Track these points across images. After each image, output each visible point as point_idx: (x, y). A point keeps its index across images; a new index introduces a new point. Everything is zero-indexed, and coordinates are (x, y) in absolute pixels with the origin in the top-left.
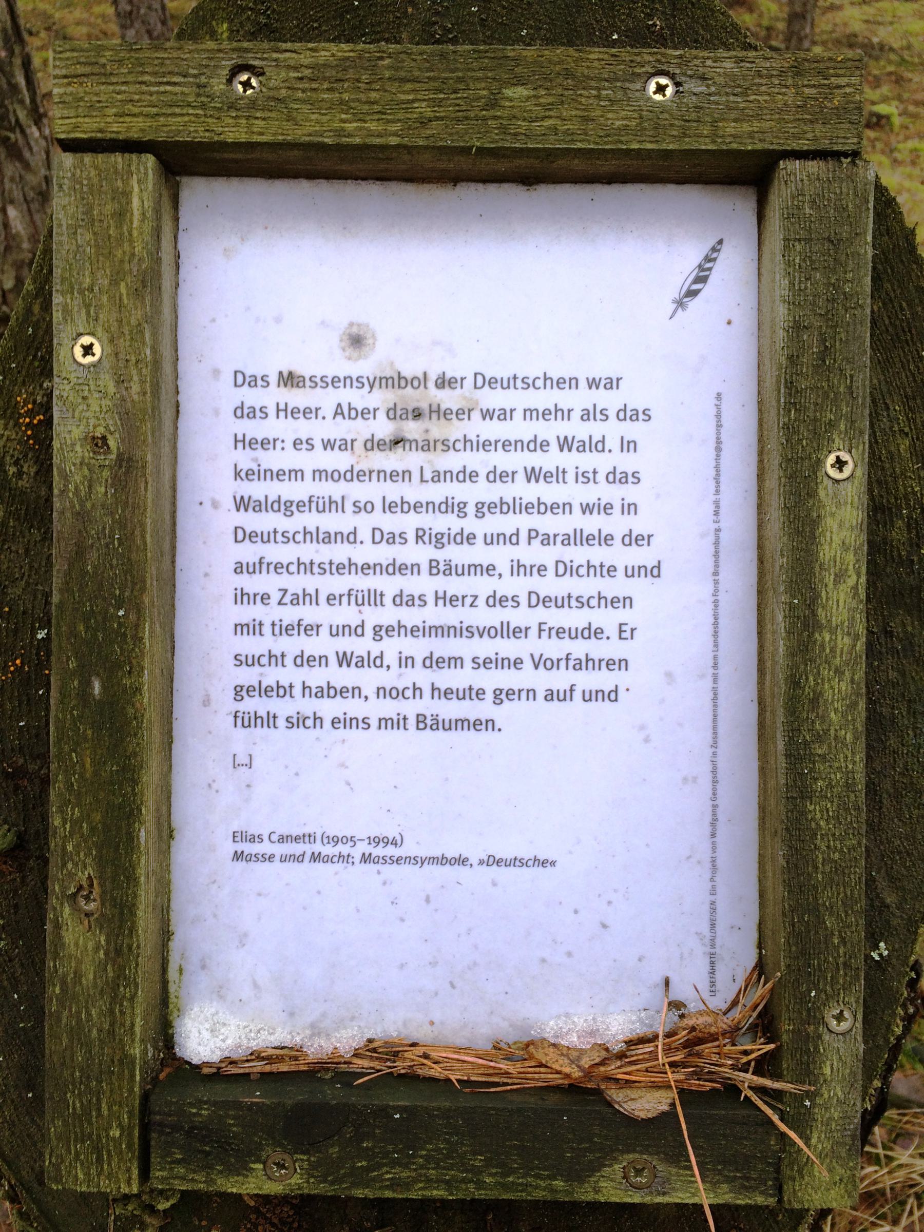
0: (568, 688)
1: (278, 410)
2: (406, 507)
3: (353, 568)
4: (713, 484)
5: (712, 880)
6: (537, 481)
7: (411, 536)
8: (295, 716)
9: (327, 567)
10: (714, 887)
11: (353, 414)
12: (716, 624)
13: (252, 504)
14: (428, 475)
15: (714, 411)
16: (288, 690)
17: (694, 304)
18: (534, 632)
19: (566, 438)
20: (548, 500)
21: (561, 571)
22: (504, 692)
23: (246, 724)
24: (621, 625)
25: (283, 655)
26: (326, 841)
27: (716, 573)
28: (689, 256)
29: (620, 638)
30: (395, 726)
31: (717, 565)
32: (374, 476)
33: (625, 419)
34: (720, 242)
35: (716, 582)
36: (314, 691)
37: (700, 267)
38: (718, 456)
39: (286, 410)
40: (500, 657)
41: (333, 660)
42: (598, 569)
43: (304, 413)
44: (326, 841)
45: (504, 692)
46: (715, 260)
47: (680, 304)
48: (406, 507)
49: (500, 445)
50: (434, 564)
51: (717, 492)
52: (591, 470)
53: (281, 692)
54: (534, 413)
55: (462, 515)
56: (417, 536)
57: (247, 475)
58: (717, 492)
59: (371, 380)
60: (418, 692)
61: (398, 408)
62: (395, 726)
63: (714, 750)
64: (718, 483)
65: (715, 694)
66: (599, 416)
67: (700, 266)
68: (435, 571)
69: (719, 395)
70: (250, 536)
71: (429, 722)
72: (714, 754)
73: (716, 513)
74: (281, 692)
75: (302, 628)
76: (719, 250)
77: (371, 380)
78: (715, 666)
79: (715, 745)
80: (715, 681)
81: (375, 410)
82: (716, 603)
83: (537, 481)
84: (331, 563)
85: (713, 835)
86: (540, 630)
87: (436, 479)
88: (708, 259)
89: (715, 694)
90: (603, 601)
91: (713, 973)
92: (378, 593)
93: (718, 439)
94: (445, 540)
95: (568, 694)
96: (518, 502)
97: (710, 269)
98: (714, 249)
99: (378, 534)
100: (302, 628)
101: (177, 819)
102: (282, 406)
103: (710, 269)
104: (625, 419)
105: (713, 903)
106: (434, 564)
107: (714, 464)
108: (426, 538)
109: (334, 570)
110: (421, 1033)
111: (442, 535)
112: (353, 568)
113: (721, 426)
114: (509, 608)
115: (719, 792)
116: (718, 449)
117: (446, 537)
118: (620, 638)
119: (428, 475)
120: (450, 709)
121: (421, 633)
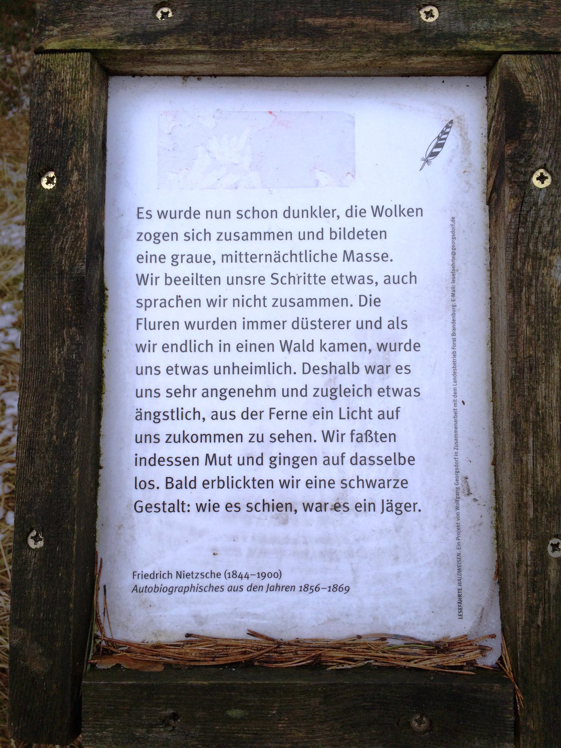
0: (395, 410)
3: (290, 437)
4: (451, 325)
5: (458, 539)
6: (381, 216)
8: (191, 232)
10: (459, 544)
11: (402, 461)
12: (455, 367)
13: (293, 346)
17: (435, 161)
18: (266, 415)
20: (189, 432)
25: (264, 299)
26: (227, 576)
27: (454, 334)
29: (139, 218)
30: (271, 508)
31: (454, 329)
32: (263, 258)
34: (451, 122)
35: (454, 340)
36: (338, 369)
38: (453, 258)
40: (367, 502)
41: (278, 347)
43: (184, 281)
44: (227, 576)
45: (300, 459)
46: (448, 133)
47: (427, 161)
50: (169, 480)
51: (454, 281)
52: (317, 320)
54: (268, 324)
57: (408, 212)
58: (454, 281)
61: (358, 457)
62: (271, 508)
63: (456, 451)
65: (456, 414)
66: (400, 326)
67: (438, 137)
71: (175, 483)
72: (456, 454)
73: (453, 295)
76: (450, 127)
79: (456, 447)
82: (454, 354)
83: (381, 216)
84: (320, 321)
86: (271, 413)
88: (443, 133)
90: (325, 257)
91: (460, 603)
92: (180, 502)
93: (453, 246)
94: (337, 393)
95: (395, 413)
97: (445, 139)
98: (447, 127)
99: (306, 366)
101: (432, 77)
103: (445, 139)
109: (204, 282)
110: (106, 385)
111: (336, 389)
114: (153, 513)
116: (454, 254)
117: (338, 391)
118: (139, 218)
119: (344, 415)
121: (244, 349)
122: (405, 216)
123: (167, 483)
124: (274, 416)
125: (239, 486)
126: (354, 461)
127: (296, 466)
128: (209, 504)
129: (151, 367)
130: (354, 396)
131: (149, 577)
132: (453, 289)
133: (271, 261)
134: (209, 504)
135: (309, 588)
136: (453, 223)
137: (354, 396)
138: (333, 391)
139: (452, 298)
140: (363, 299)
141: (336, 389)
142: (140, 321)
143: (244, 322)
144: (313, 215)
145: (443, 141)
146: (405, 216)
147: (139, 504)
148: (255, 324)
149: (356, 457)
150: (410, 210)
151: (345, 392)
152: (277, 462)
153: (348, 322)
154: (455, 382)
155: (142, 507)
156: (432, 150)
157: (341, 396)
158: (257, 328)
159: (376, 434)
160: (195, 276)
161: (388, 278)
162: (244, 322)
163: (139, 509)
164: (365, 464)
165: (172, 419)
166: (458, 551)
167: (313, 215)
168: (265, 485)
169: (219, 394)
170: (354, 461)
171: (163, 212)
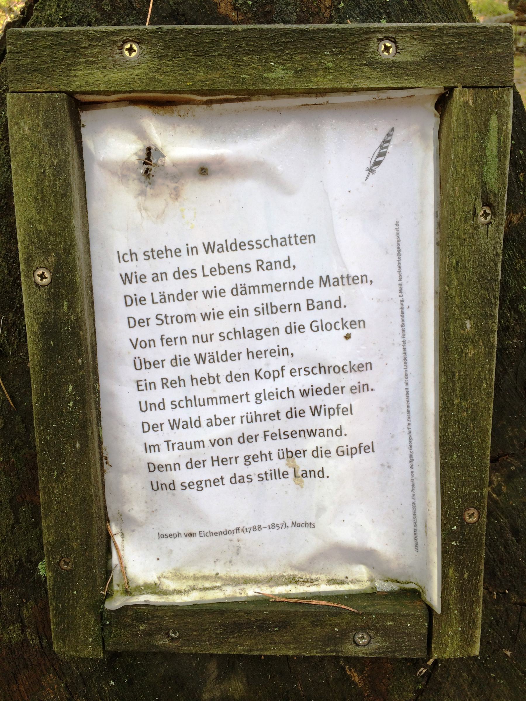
1: (213, 461)
2: (222, 271)
3: (169, 252)
5: (412, 491)
7: (253, 266)
9: (150, 254)
11: (274, 310)
13: (216, 247)
14: (157, 299)
15: (395, 232)
16: (216, 378)
17: (378, 170)
19: (209, 243)
21: (129, 302)
22: (263, 331)
23: (250, 420)
24: (265, 432)
27: (403, 325)
28: (374, 141)
29: (139, 390)
31: (403, 321)
33: (236, 483)
34: (392, 130)
37: (381, 147)
38: (399, 258)
39: (218, 461)
42: (268, 456)
45: (263, 331)
46: (389, 141)
47: (371, 171)
48: (222, 271)
49: (268, 353)
50: (310, 302)
51: (400, 279)
52: (263, 473)
53: (212, 380)
54: (269, 287)
55: (200, 489)
56: (258, 266)
57: (351, 325)
58: (400, 279)
59: (213, 442)
60: (134, 256)
61: (237, 477)
63: (409, 422)
64: (400, 273)
68: (311, 307)
69: (397, 222)
70: (153, 428)
72: (411, 453)
73: (401, 291)
74: (212, 380)
75: (340, 410)
76: (391, 136)
77: (213, 442)
78: (406, 376)
80: (407, 385)
81: (204, 461)
84: (152, 251)
85: (412, 468)
86: (265, 436)
87: (163, 300)
89: (401, 288)
94: (262, 398)
96: (178, 358)
98: (388, 135)
99: (146, 426)
100: (340, 410)
102: (215, 458)
104: (236, 483)
105: (414, 503)
106: (310, 302)
107: (397, 263)
108: (264, 266)
109: (155, 256)
111: (260, 394)
112: (169, 252)
113: (399, 241)
115: (413, 445)
116: (399, 254)
117: (262, 395)
118: (139, 390)
119: (157, 299)
120: (227, 259)
121: (236, 315)
122: (262, 378)
123: (308, 305)
124: (269, 438)
125: (283, 396)
126: (233, 480)
127: (259, 338)
128: (214, 313)
129: (241, 266)
130: (277, 398)
131: (323, 392)
132: (401, 286)
133: (277, 246)
134: (216, 290)
135: (276, 525)
136: (397, 227)
137: (277, 398)
138: (259, 331)
139: (400, 294)
140: (128, 299)
141: (260, 394)
142: (140, 383)
143: (188, 248)
144: (260, 268)
145: (385, 150)
146: (262, 378)
147: (314, 324)
148: (256, 288)
149: (235, 477)
150: (169, 340)
151: (269, 396)
152: (203, 485)
153: (256, 436)
154: (406, 365)
155: (317, 327)
156: (376, 159)
157: (265, 399)
158: (259, 292)
159: (166, 317)
160: (273, 472)
161: (155, 275)
162: (188, 248)
163: (315, 329)
164: (244, 482)
165: (291, 244)
166: (401, 298)
167: (260, 268)
168: (235, 271)
169: (255, 334)
170: (233, 480)
171: (207, 291)
